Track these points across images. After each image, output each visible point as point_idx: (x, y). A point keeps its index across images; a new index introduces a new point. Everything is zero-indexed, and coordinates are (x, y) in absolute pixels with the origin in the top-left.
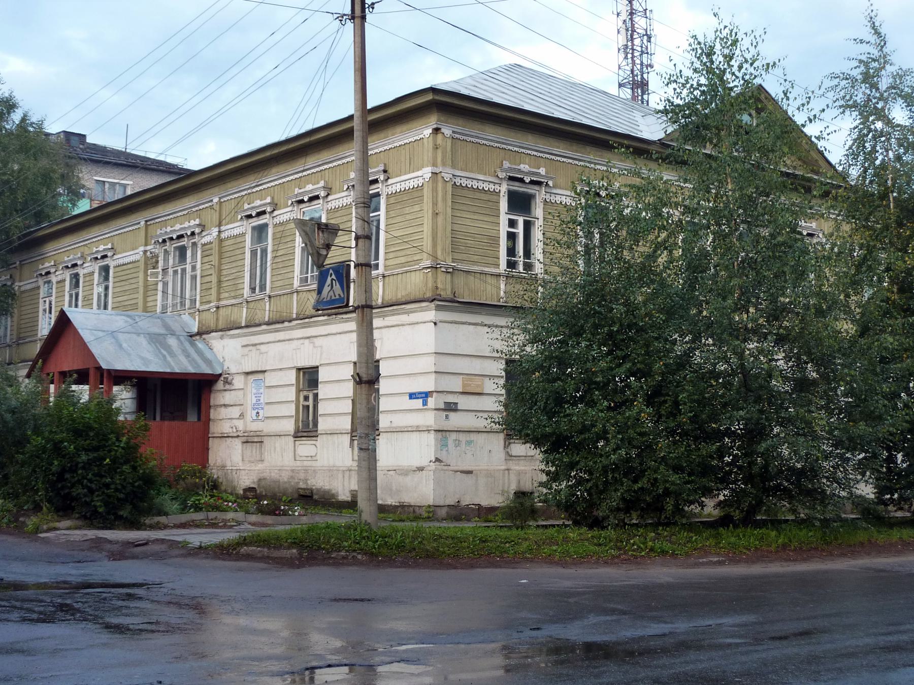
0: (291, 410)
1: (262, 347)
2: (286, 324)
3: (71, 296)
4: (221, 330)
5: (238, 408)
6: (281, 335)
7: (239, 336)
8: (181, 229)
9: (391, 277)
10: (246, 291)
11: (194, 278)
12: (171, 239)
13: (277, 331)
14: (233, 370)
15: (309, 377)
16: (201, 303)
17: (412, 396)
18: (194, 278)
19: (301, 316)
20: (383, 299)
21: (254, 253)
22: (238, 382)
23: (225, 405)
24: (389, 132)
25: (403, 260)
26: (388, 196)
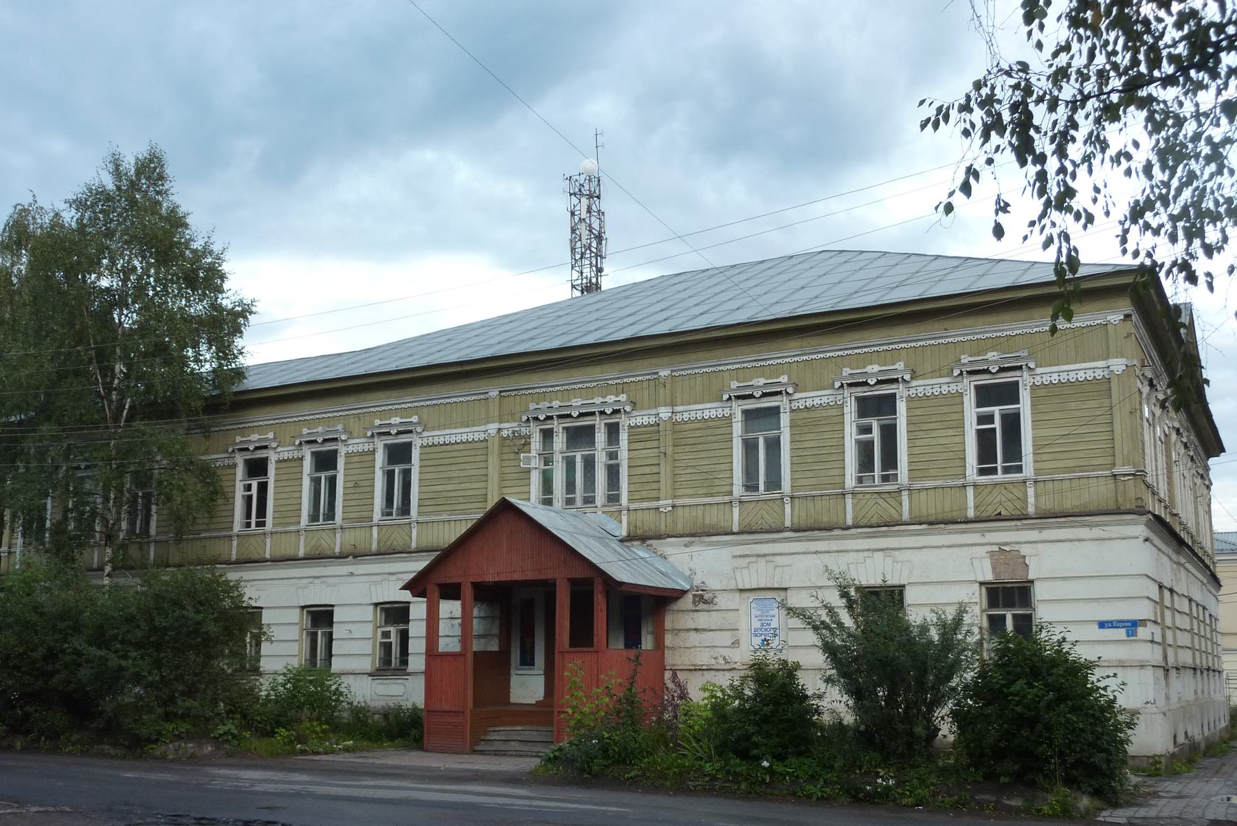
0: (367, 648)
1: (779, 559)
2: (837, 532)
3: (570, 464)
4: (688, 535)
5: (729, 633)
6: (822, 545)
7: (727, 544)
8: (259, 440)
9: (923, 494)
10: (738, 490)
11: (613, 473)
12: (602, 413)
13: (774, 541)
14: (713, 584)
15: (321, 617)
16: (420, 513)
17: (1102, 625)
18: (613, 473)
19: (864, 522)
20: (1036, 507)
21: (750, 448)
22: (723, 601)
23: (696, 630)
24: (693, 356)
25: (1070, 463)
26: (348, 455)
